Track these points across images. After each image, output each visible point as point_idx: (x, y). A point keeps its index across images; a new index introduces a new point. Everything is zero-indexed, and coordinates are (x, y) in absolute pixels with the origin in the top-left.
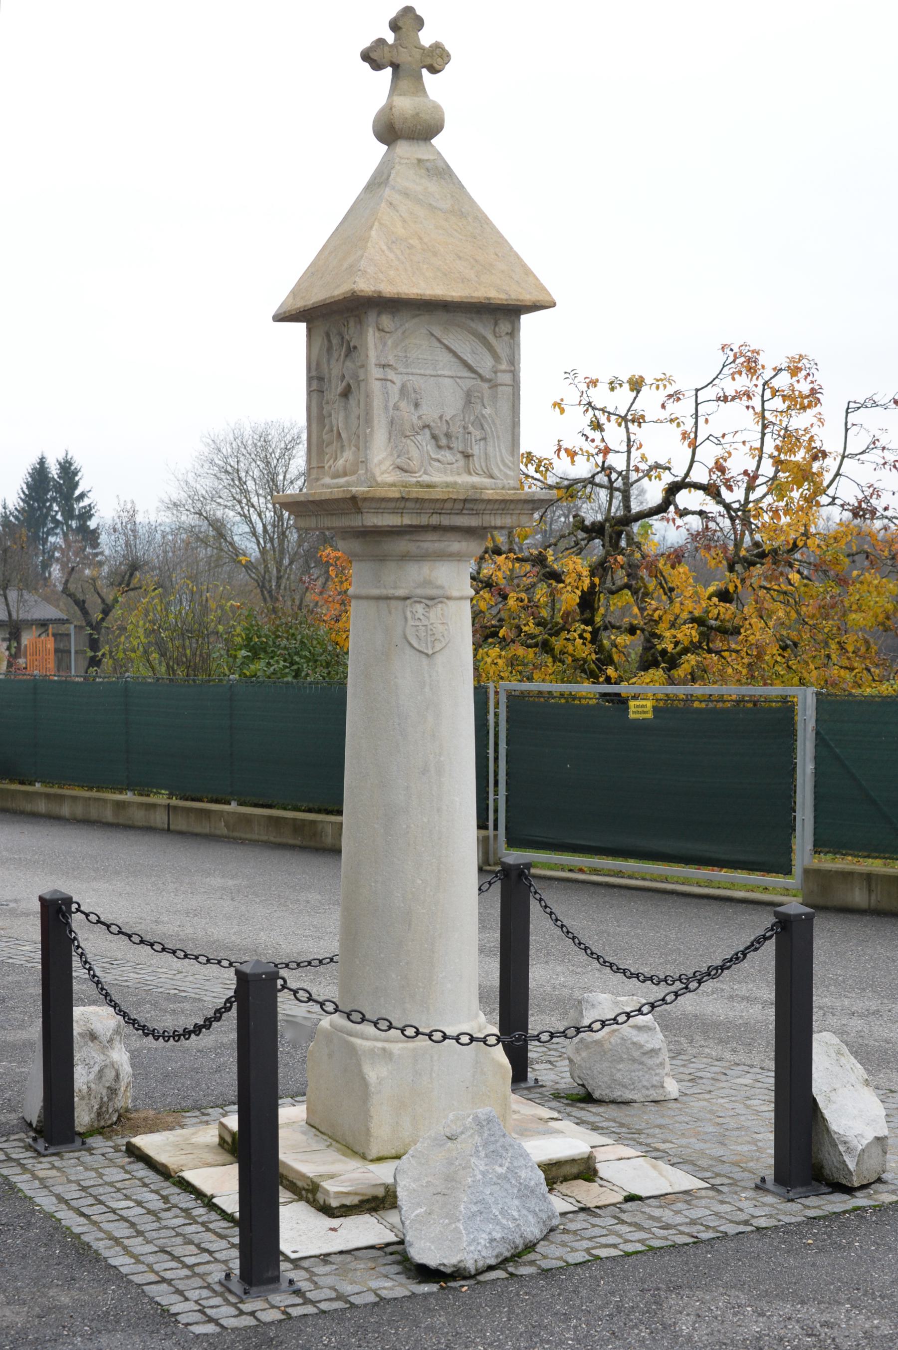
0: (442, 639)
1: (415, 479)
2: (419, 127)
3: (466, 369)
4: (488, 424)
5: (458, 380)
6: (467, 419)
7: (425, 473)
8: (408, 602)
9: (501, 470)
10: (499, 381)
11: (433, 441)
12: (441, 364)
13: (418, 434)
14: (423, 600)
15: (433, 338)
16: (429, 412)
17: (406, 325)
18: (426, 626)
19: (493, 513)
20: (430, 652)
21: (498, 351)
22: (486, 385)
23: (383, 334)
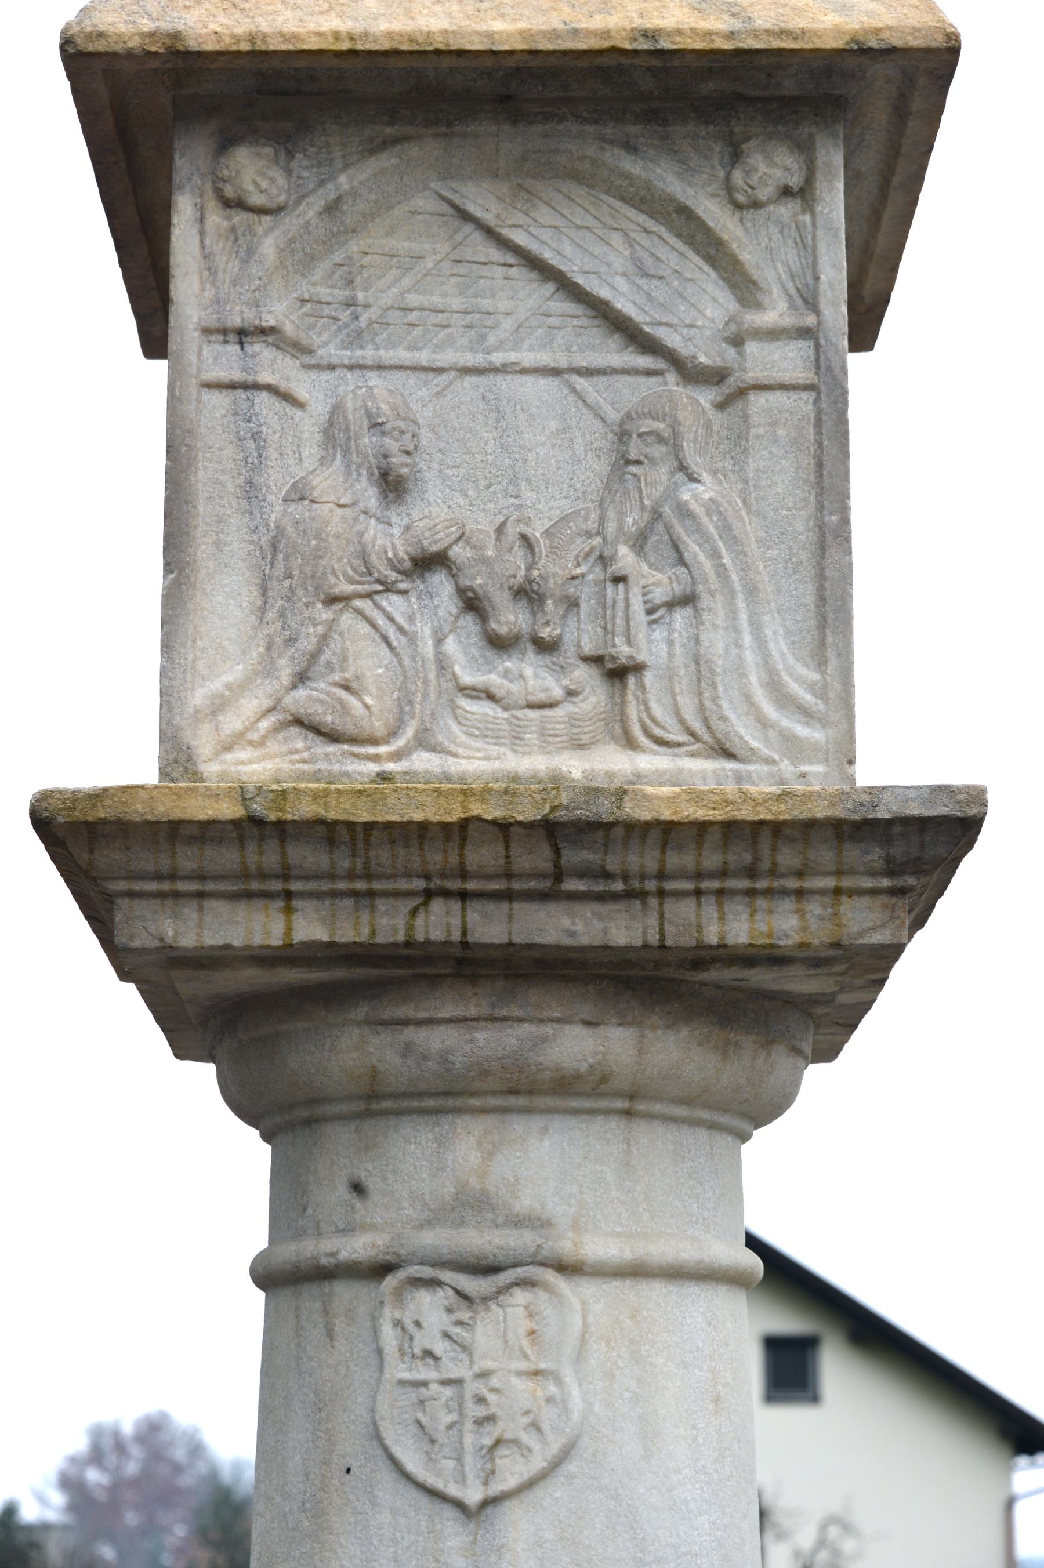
0: (528, 1439)
1: (373, 768)
3: (615, 341)
4: (705, 538)
5: (581, 383)
6: (611, 526)
7: (423, 741)
8: (390, 1281)
9: (764, 723)
10: (754, 374)
11: (469, 622)
12: (508, 324)
13: (389, 588)
14: (446, 1276)
15: (469, 228)
16: (436, 511)
18: (458, 1382)
19: (709, 887)
20: (473, 1496)
21: (745, 257)
22: (705, 397)
23: (240, 218)
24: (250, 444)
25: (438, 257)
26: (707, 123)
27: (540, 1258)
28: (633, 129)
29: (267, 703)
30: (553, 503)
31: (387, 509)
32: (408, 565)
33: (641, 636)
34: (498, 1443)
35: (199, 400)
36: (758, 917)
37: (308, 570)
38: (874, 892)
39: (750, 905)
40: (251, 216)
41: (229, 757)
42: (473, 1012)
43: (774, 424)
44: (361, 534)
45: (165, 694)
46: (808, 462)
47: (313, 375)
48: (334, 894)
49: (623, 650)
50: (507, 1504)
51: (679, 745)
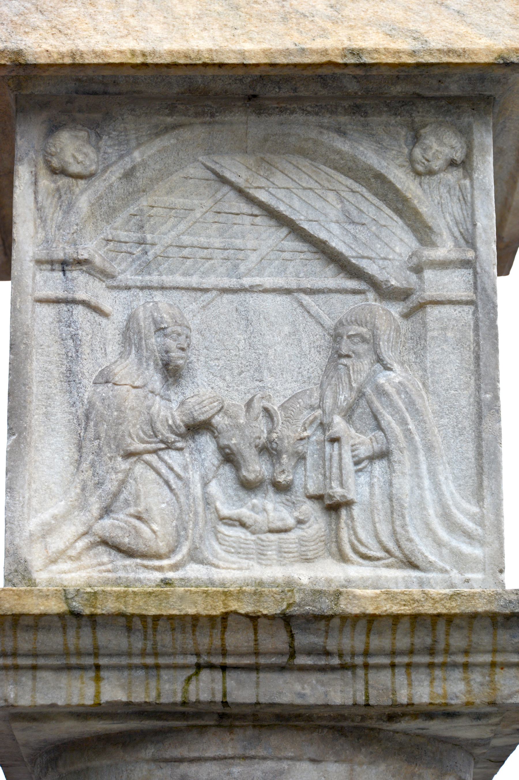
1: (158, 576)
5: (306, 299)
6: (329, 402)
7: (195, 557)
9: (439, 543)
10: (430, 293)
11: (227, 470)
12: (254, 257)
13: (169, 446)
15: (226, 189)
16: (201, 392)
17: (136, 154)
21: (423, 209)
22: (395, 310)
23: (63, 181)
24: (70, 342)
28: (343, 119)
29: (82, 529)
30: (287, 385)
31: (168, 389)
32: (183, 429)
35: (33, 312)
36: (436, 683)
39: (430, 674)
41: (54, 568)
42: (230, 752)
43: (444, 329)
46: (469, 356)
47: (115, 293)
48: (130, 667)
51: (378, 559)
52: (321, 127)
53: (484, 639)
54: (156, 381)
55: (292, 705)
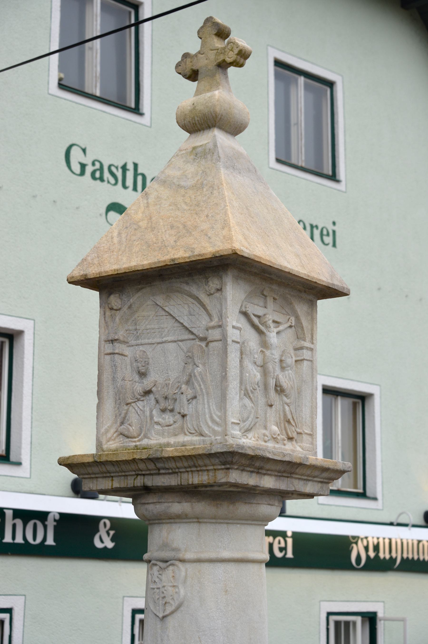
0: (171, 602)
1: (134, 444)
2: (196, 119)
3: (187, 332)
4: (198, 382)
5: (180, 343)
7: (146, 437)
9: (209, 427)
12: (166, 331)
13: (139, 400)
14: (158, 563)
15: (159, 307)
17: (131, 300)
19: (189, 470)
23: (113, 312)
24: (114, 368)
25: (153, 316)
26: (201, 275)
27: (175, 558)
28: (186, 279)
29: (115, 430)
30: (175, 374)
31: (142, 379)
32: (142, 394)
33: (185, 408)
34: (166, 603)
35: (104, 358)
36: (200, 476)
37: (123, 397)
38: (222, 469)
39: (198, 474)
40: (115, 311)
41: (108, 443)
42: (155, 501)
43: (214, 351)
44: (133, 388)
45: (97, 429)
47: (129, 348)
48: (120, 476)
49: (186, 413)
50: (168, 617)
51: (194, 434)
52: (181, 282)
53: (207, 461)
54: (137, 378)
55: (162, 486)
